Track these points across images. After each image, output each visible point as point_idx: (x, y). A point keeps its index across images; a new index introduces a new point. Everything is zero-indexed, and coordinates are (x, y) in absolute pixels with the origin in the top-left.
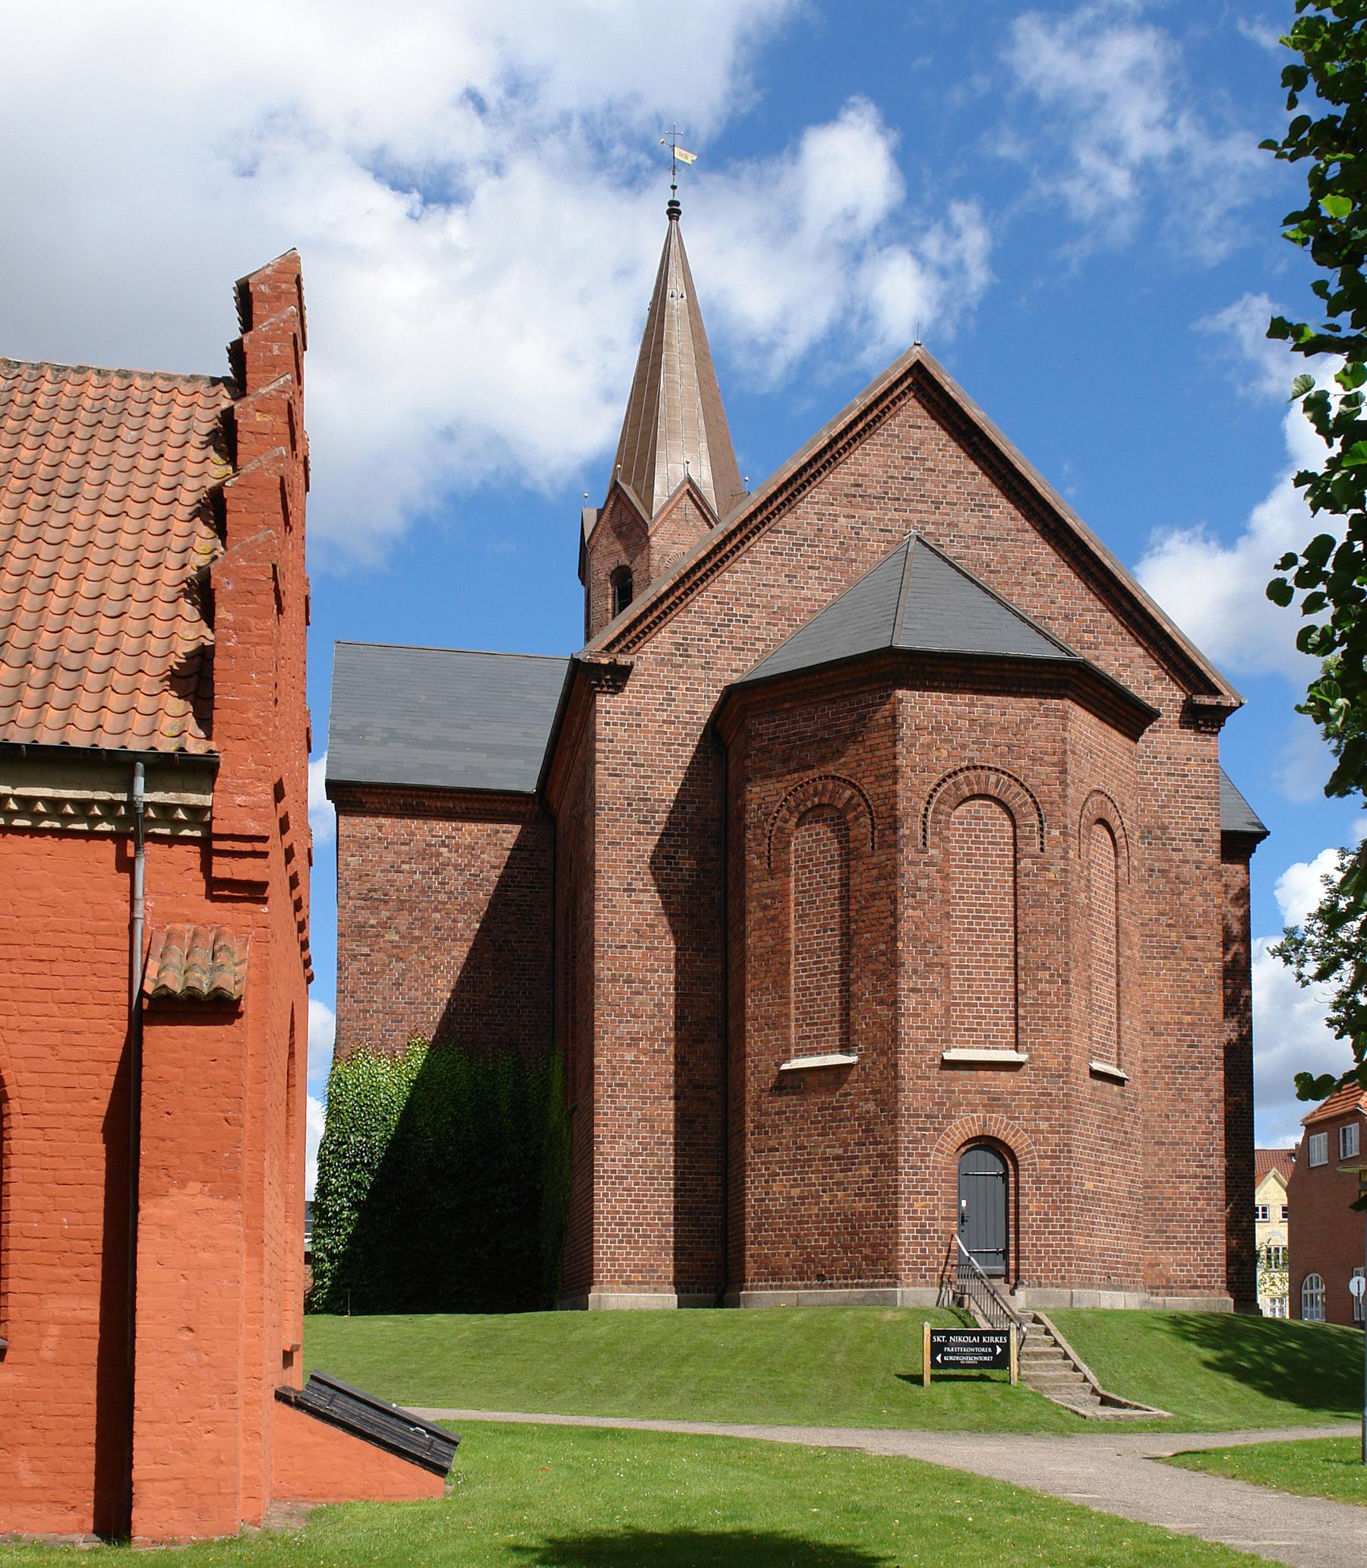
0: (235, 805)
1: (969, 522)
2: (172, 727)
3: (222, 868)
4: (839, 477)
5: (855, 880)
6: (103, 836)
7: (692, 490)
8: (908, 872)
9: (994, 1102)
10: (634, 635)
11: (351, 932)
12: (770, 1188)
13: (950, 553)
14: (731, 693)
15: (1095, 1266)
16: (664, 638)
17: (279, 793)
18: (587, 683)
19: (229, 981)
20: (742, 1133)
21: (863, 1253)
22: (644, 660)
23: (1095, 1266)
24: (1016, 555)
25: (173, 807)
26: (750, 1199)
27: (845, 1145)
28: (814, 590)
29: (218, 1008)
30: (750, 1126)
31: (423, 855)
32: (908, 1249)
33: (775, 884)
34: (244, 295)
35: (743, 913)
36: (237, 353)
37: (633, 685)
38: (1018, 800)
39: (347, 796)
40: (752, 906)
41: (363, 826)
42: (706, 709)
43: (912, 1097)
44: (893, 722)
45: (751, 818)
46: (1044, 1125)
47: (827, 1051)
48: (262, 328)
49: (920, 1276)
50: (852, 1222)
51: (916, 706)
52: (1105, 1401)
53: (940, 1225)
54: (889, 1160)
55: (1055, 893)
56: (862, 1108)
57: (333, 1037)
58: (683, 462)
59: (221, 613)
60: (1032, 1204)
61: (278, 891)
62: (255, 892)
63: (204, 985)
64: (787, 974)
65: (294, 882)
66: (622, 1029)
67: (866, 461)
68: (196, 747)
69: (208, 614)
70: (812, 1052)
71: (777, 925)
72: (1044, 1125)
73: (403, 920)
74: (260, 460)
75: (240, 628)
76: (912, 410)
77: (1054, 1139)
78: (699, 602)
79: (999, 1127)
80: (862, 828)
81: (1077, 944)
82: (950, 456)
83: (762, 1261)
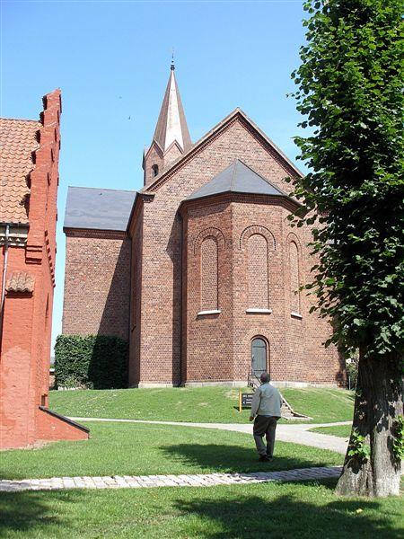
0: (34, 238)
1: (254, 156)
2: (19, 216)
3: (30, 255)
4: (217, 143)
5: (220, 258)
6: (21, 247)
7: (176, 144)
8: (236, 256)
9: (262, 324)
10: (156, 186)
11: (69, 272)
12: (194, 352)
13: (248, 164)
14: (183, 203)
15: (293, 375)
16: (164, 187)
17: (46, 234)
18: (141, 199)
19: (30, 286)
20: (186, 334)
21: (222, 371)
22: (158, 194)
23: (293, 375)
24: (268, 165)
25: (16, 238)
26: (188, 355)
27: (217, 338)
28: (209, 174)
29: (27, 294)
30: (188, 332)
31: (91, 249)
32: (236, 369)
33: (196, 259)
34: (45, 100)
35: (186, 266)
36: (42, 115)
37: (155, 200)
38: (266, 233)
39: (69, 231)
40: (189, 265)
41: (74, 240)
42: (177, 208)
43: (238, 323)
44: (231, 212)
45: (189, 239)
46: (277, 332)
47: (212, 309)
48: (49, 109)
49: (241, 377)
50: (219, 361)
51: (237, 207)
52: (295, 415)
53: (246, 362)
54: (230, 342)
55: (279, 262)
56: (223, 323)
57: (70, 308)
58: (174, 134)
59: (32, 186)
60: (274, 355)
61: (45, 262)
62: (38, 261)
63: (23, 289)
64: (199, 286)
65: (50, 258)
66: (150, 302)
67: (224, 139)
68: (24, 222)
69: (29, 186)
70: (207, 309)
71: (197, 272)
72: (277, 332)
73: (85, 269)
74: (47, 142)
75: (38, 190)
76: (237, 125)
77: (280, 336)
78: (175, 177)
79: (263, 332)
80: (222, 242)
81: (287, 277)
82: (249, 138)
83: (192, 374)
